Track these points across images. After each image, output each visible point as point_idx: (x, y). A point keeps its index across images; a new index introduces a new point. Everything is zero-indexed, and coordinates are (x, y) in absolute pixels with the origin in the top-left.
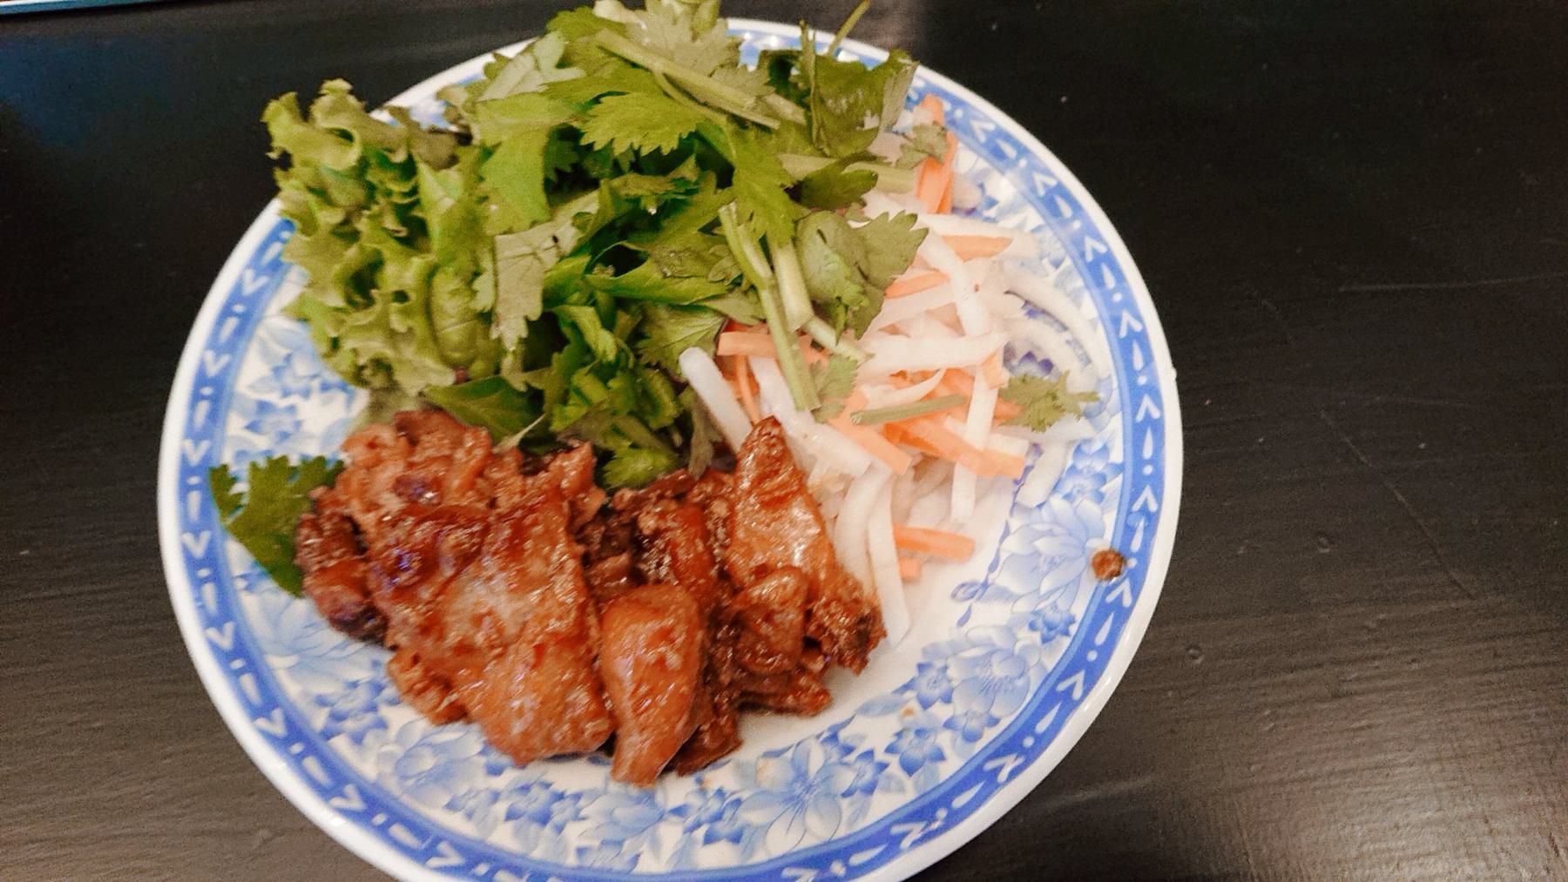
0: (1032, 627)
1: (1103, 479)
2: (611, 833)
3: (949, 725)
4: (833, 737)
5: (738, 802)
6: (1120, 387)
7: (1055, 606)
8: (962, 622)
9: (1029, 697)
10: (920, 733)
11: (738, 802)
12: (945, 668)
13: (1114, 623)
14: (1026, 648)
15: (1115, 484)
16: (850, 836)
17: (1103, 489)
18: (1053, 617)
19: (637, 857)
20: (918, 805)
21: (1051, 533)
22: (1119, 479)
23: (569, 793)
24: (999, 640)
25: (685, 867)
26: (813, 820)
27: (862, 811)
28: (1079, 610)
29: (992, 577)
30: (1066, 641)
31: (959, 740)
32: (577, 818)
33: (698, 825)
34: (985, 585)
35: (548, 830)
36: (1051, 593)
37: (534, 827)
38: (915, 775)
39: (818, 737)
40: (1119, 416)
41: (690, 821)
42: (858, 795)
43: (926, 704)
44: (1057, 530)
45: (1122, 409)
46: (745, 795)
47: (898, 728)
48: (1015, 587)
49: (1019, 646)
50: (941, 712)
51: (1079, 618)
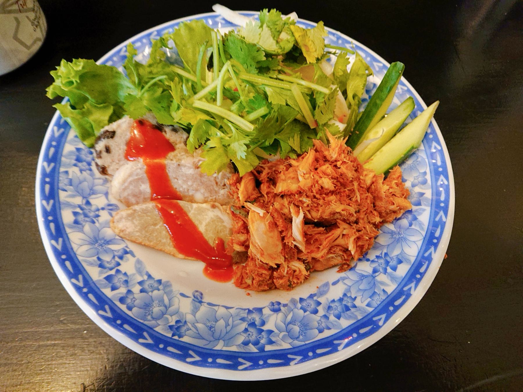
0: (177, 322)
1: (256, 343)
2: (75, 182)
3: (129, 292)
4: (126, 252)
5: (94, 222)
6: (306, 344)
7: (189, 329)
8: (182, 295)
9: (142, 321)
10: (126, 282)
11: (94, 222)
12: (159, 290)
13: (94, 303)
14: (167, 319)
15: (253, 349)
16: (79, 262)
17: (250, 345)
18: (183, 329)
19: (66, 191)
20: (90, 282)
21: (227, 325)
22: (256, 350)
23: (341, 297)
24: (171, 309)
25: (62, 206)
26: (85, 248)
27: (91, 264)
28: (186, 339)
29: (205, 304)
30: (170, 335)
31: (121, 295)
32: (81, 171)
33: (82, 209)
34: (201, 302)
35: (74, 162)
36: (196, 328)
37: (75, 157)
38: (105, 280)
39: (127, 247)
40: (290, 347)
41: (84, 207)
42: (99, 262)
43: (140, 283)
44: (229, 328)
45: (294, 348)
46: (97, 224)
47: (128, 274)
48: (198, 315)
49: (169, 317)
50: (136, 289)
51: (181, 339)
